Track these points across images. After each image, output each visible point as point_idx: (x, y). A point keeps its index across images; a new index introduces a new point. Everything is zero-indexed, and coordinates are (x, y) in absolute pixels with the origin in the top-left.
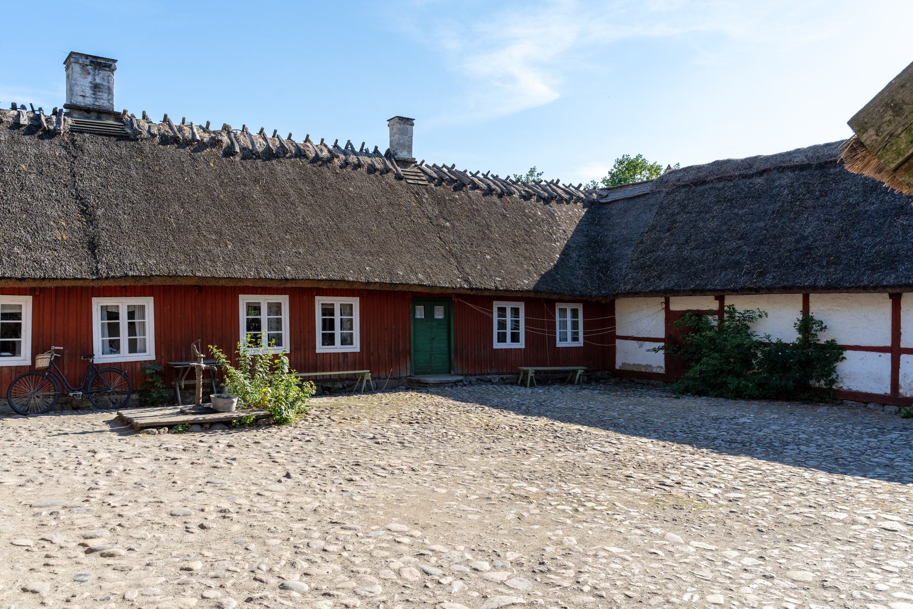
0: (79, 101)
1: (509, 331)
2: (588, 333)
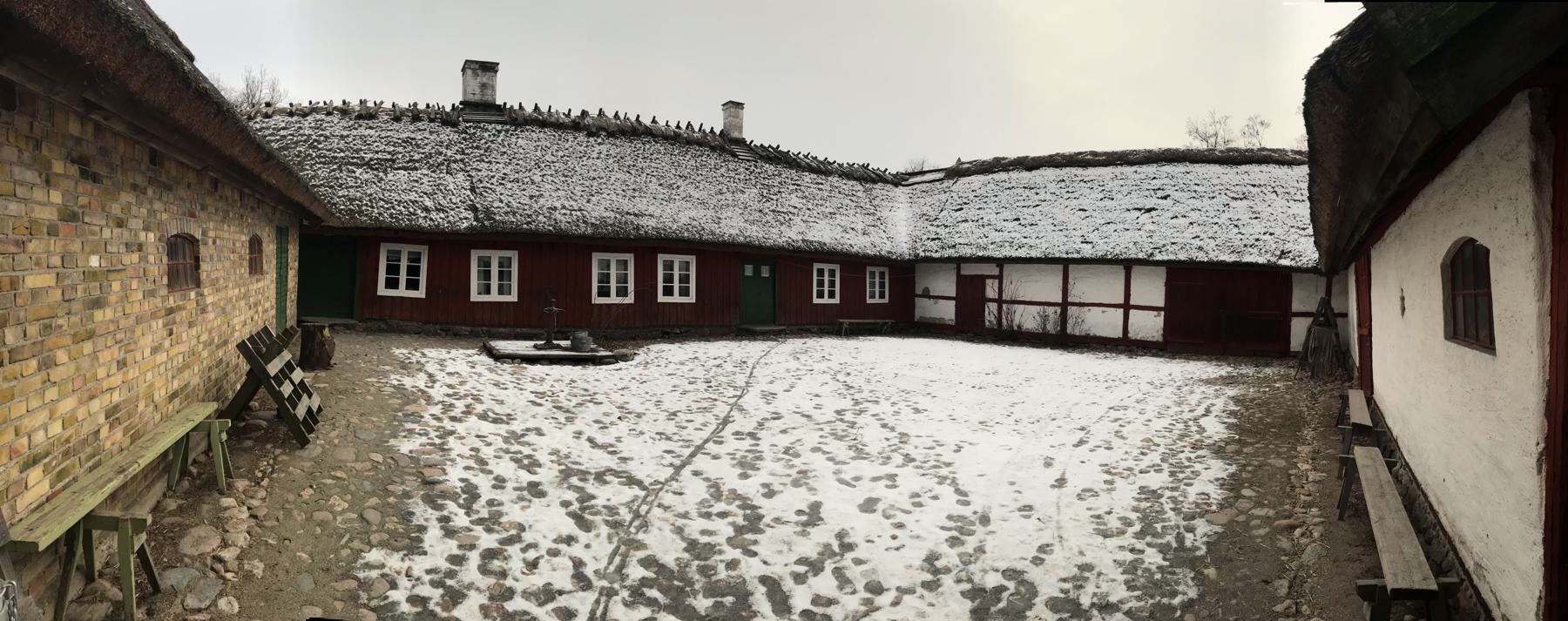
0: (471, 98)
1: (826, 289)
2: (261, 338)
